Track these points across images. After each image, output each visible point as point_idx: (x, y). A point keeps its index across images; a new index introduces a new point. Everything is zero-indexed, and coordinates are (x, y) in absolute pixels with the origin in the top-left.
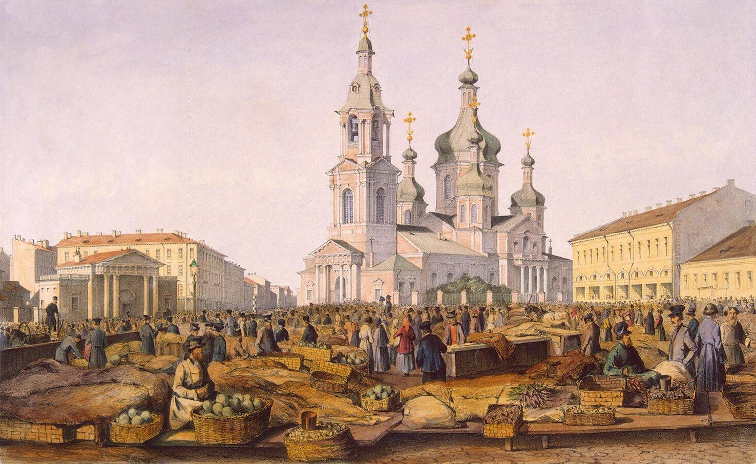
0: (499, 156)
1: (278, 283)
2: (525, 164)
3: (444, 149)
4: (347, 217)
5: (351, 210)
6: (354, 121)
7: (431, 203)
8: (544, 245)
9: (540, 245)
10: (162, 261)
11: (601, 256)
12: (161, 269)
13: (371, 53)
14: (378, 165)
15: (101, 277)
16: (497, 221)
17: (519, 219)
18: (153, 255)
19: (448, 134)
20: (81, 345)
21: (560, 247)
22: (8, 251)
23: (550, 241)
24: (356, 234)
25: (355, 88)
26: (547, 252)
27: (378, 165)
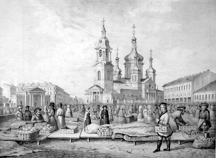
0: (143, 62)
1: (79, 97)
2: (117, 60)
3: (127, 59)
4: (99, 79)
5: (100, 78)
6: (101, 51)
7: (123, 76)
8: (155, 87)
9: (154, 87)
10: (46, 90)
11: (176, 89)
12: (46, 93)
13: (105, 31)
14: (109, 64)
15: (148, 93)
16: (142, 80)
17: (148, 79)
18: (43, 89)
19: (128, 56)
20: (114, 106)
21: (161, 88)
22: (2, 87)
23: (157, 86)
24: (102, 83)
25: (101, 42)
26: (156, 89)
27: (109, 64)
